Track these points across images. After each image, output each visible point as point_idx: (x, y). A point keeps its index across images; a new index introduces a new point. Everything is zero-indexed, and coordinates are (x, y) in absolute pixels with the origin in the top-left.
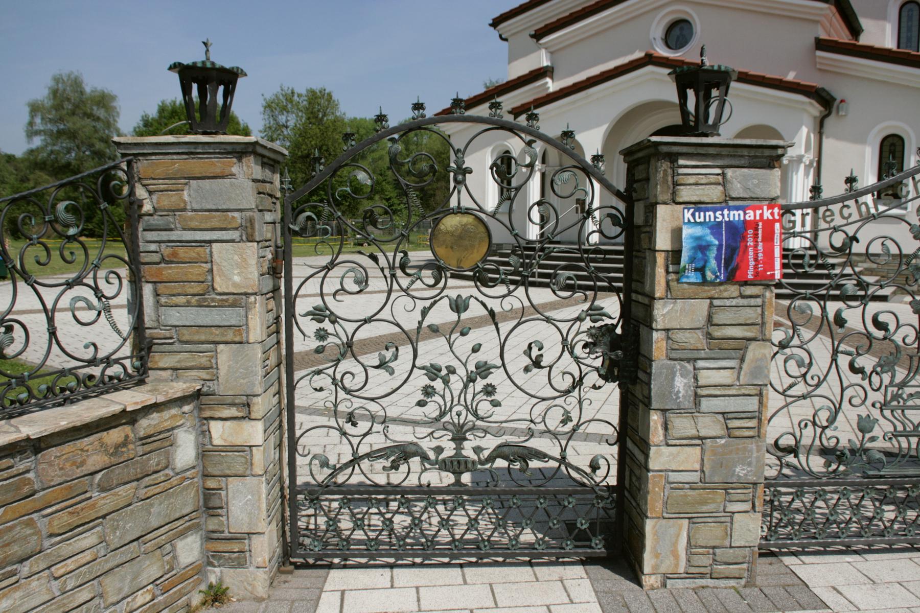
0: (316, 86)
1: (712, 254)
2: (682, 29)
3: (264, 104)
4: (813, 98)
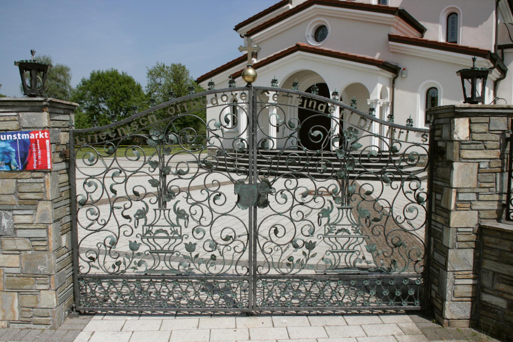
0: (176, 62)
1: (13, 156)
3: (148, 72)
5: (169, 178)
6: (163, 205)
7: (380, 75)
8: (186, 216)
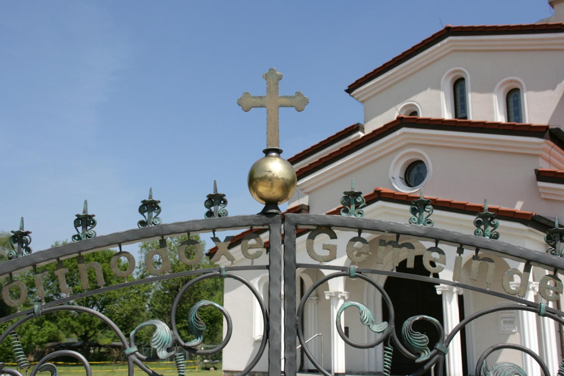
2: (419, 169)
4: (531, 226)
7: (528, 238)
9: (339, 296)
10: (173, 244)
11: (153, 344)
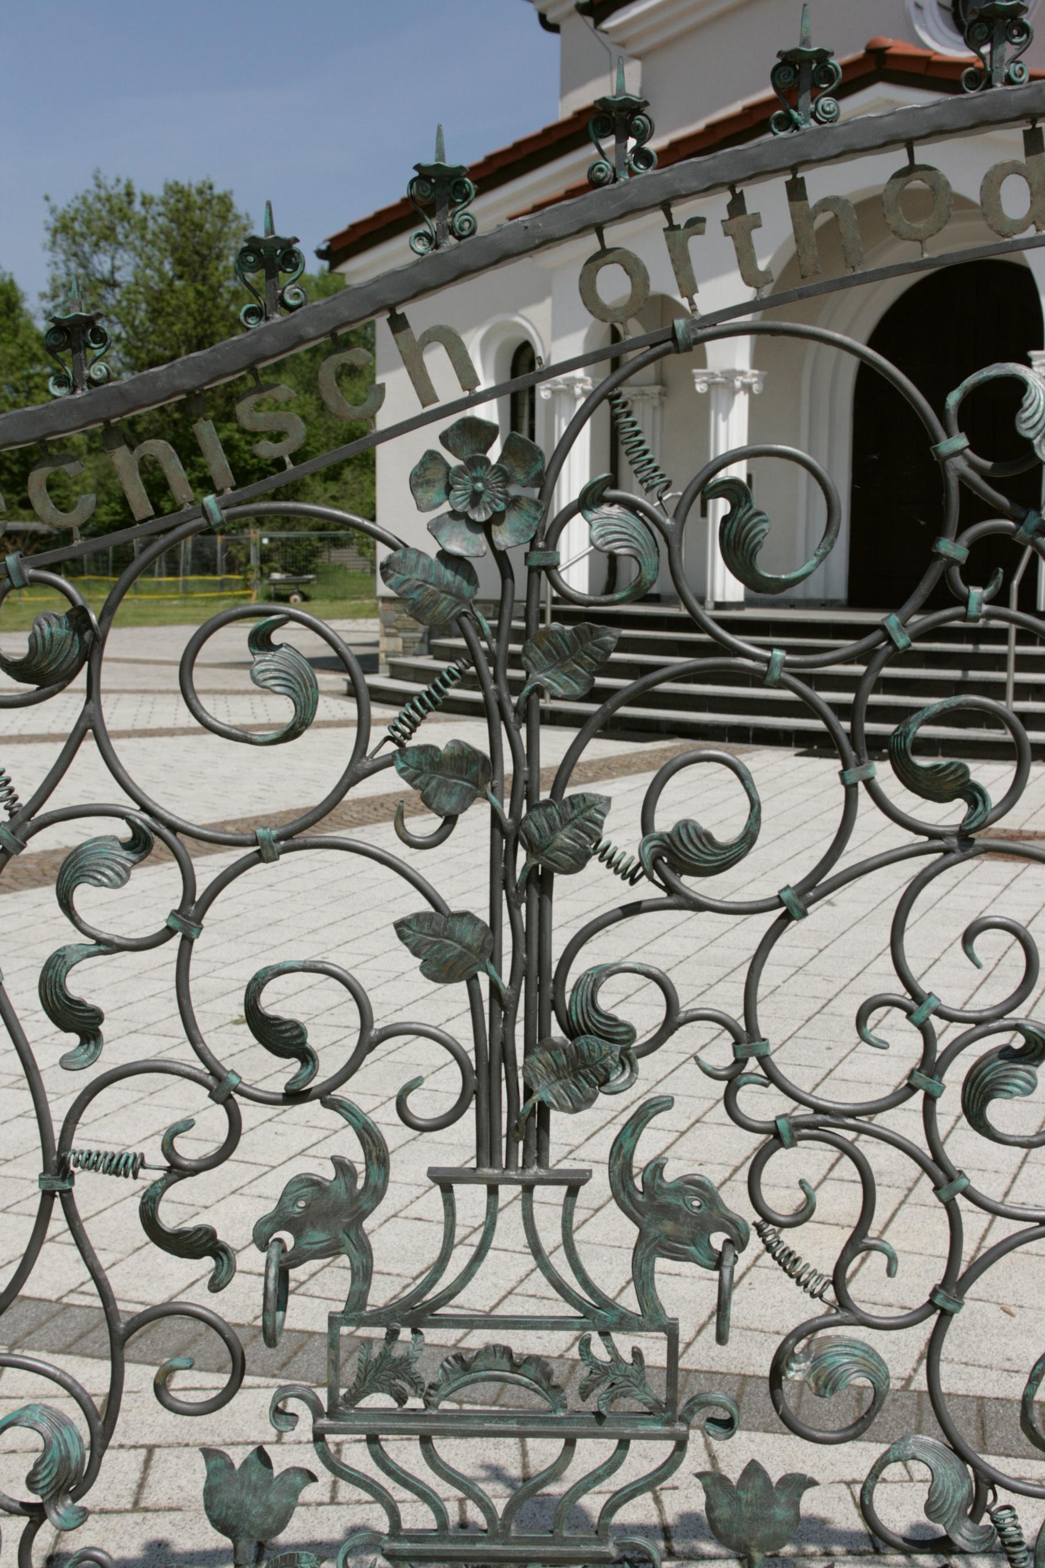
0: (190, 178)
5: (578, 896)
6: (512, 1137)
8: (717, 1240)
9: (738, 384)
10: (151, 223)
11: (1024, 426)
